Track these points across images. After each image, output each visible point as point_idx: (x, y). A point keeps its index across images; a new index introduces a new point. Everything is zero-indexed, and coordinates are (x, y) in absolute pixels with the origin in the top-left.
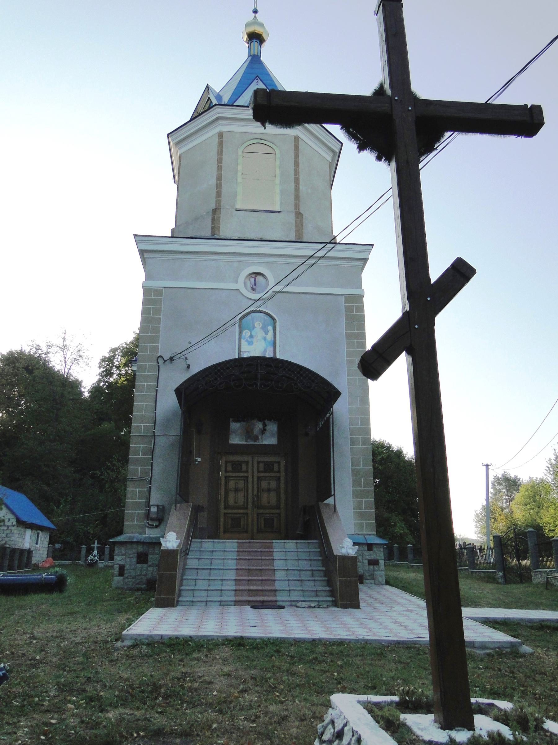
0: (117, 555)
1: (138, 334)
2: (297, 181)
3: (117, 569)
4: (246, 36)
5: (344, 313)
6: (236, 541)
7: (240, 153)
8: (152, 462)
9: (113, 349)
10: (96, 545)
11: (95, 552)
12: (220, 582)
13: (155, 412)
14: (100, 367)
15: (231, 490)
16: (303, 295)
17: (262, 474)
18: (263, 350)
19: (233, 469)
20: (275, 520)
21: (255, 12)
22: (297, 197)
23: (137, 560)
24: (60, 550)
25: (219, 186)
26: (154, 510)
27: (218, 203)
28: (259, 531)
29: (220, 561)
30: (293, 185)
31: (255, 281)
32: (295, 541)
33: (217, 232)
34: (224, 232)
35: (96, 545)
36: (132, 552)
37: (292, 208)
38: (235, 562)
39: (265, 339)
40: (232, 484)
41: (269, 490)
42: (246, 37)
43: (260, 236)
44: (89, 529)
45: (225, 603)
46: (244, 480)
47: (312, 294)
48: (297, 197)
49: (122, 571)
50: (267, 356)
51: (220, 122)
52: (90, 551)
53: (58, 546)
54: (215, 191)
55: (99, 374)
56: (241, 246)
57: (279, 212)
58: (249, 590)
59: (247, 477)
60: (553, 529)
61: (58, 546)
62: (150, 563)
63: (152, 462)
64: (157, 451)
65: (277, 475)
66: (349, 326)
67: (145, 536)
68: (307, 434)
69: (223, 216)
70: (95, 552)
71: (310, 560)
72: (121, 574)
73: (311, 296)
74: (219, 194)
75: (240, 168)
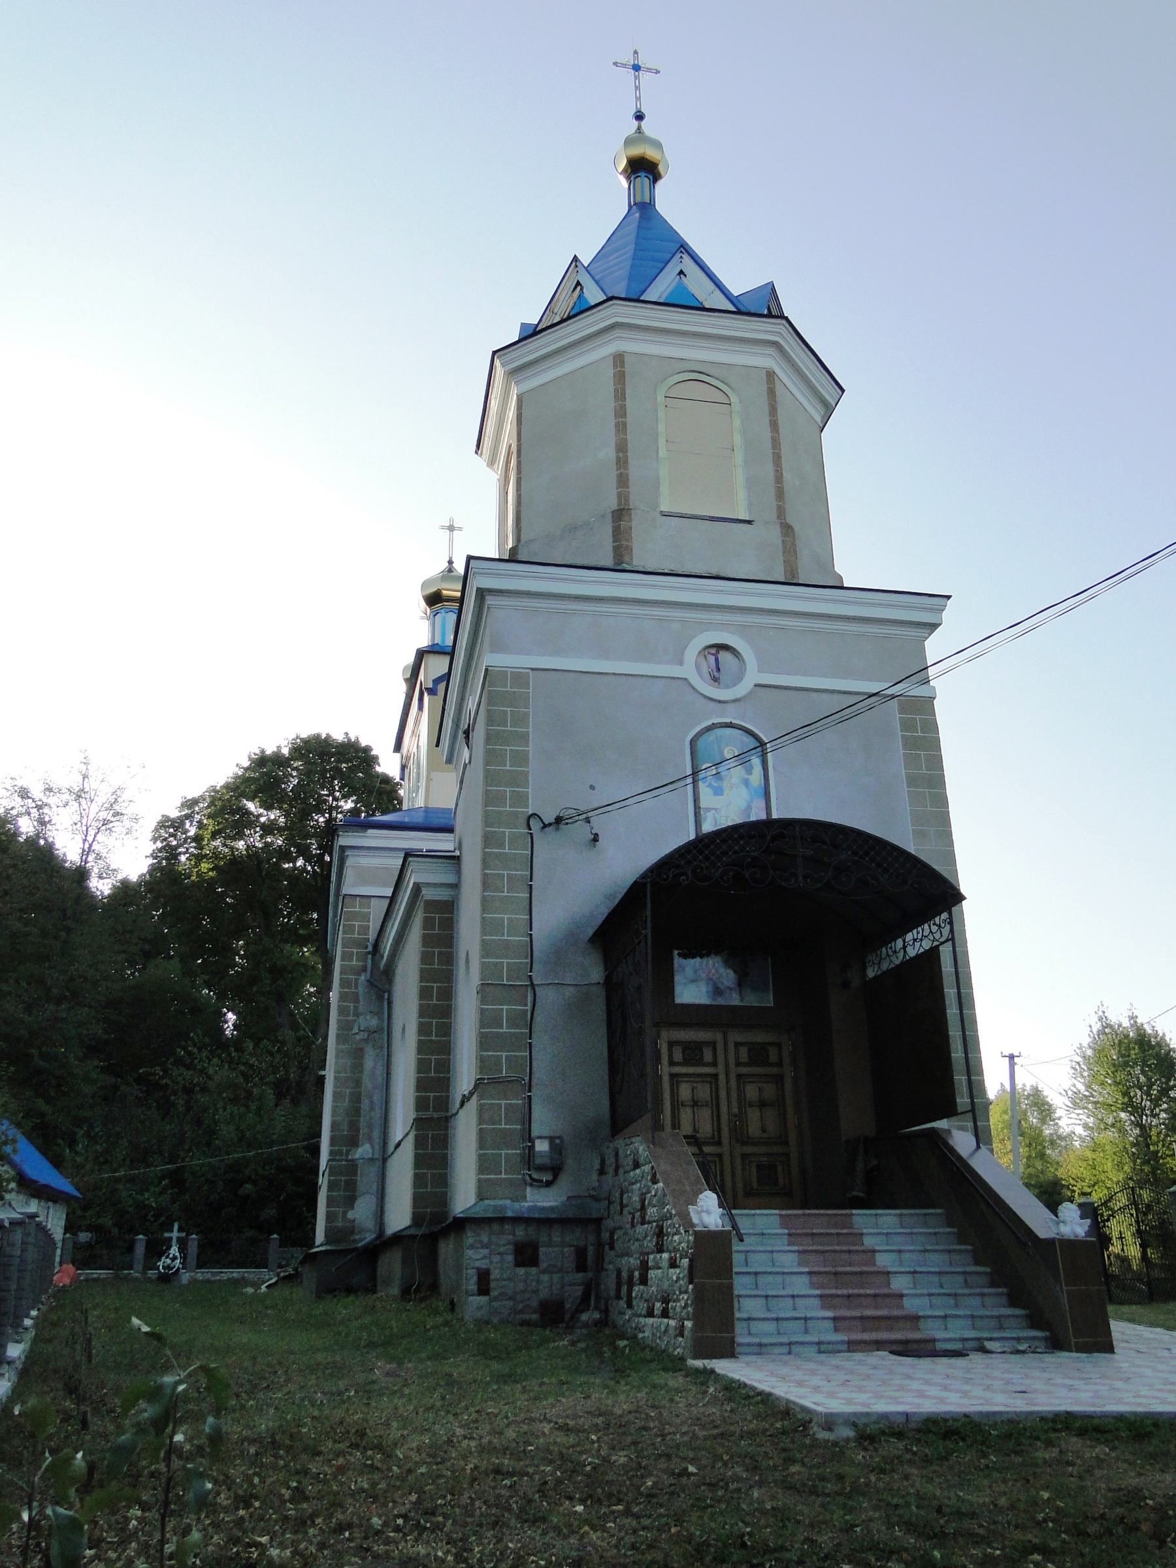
0: (472, 1247)
1: (246, 769)
2: (777, 459)
3: (474, 1279)
4: (625, 162)
5: (900, 733)
6: (777, 1212)
7: (661, 398)
8: (530, 1044)
9: (189, 800)
10: (175, 1234)
11: (174, 1250)
12: (789, 1301)
13: (531, 935)
14: (155, 840)
15: (750, 1106)
16: (815, 695)
17: (744, 1070)
18: (743, 805)
19: (684, 1058)
20: (780, 1169)
21: (639, 117)
22: (780, 494)
23: (516, 1259)
24: (89, 1246)
25: (622, 462)
26: (542, 1146)
27: (623, 497)
28: (749, 1193)
29: (764, 1256)
30: (770, 467)
31: (717, 660)
32: (897, 1211)
33: (626, 558)
34: (642, 554)
35: (175, 1234)
36: (505, 1240)
37: (772, 515)
38: (794, 1257)
39: (746, 783)
40: (685, 1091)
41: (695, 1104)
42: (623, 163)
43: (714, 571)
44: (148, 1199)
45: (830, 1347)
46: (744, 1082)
47: (833, 692)
48: (780, 494)
49: (484, 1283)
50: (753, 818)
51: (617, 333)
52: (157, 1249)
53: (84, 1237)
54: (613, 474)
55: (152, 855)
56: (695, 590)
57: (749, 522)
58: (862, 1318)
59: (716, 1076)
60: (1089, 1190)
61: (84, 1237)
62: (543, 1265)
63: (530, 1044)
64: (539, 1019)
65: (775, 1070)
66: (911, 761)
67: (526, 1204)
68: (846, 985)
69: (638, 525)
70: (174, 1250)
71: (949, 1251)
72: (484, 1288)
73: (830, 696)
74: (623, 481)
75: (661, 428)
